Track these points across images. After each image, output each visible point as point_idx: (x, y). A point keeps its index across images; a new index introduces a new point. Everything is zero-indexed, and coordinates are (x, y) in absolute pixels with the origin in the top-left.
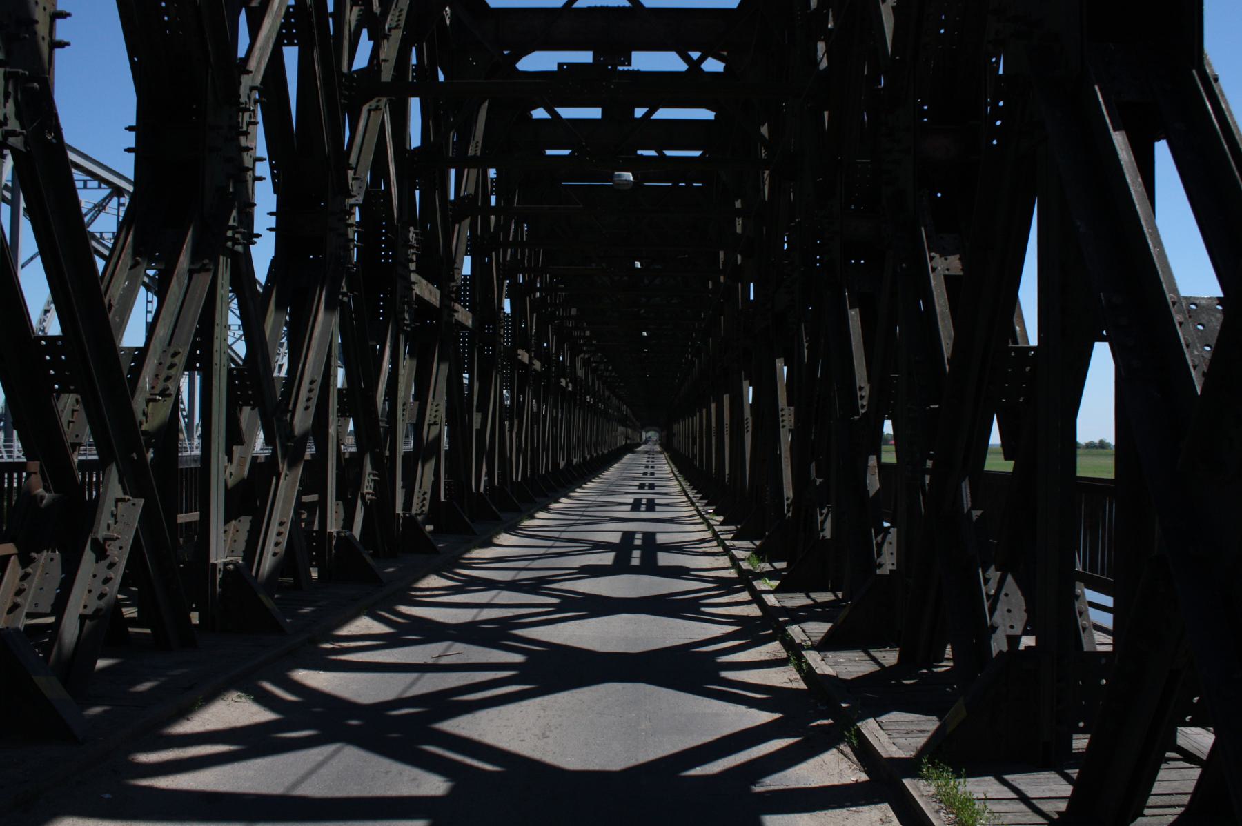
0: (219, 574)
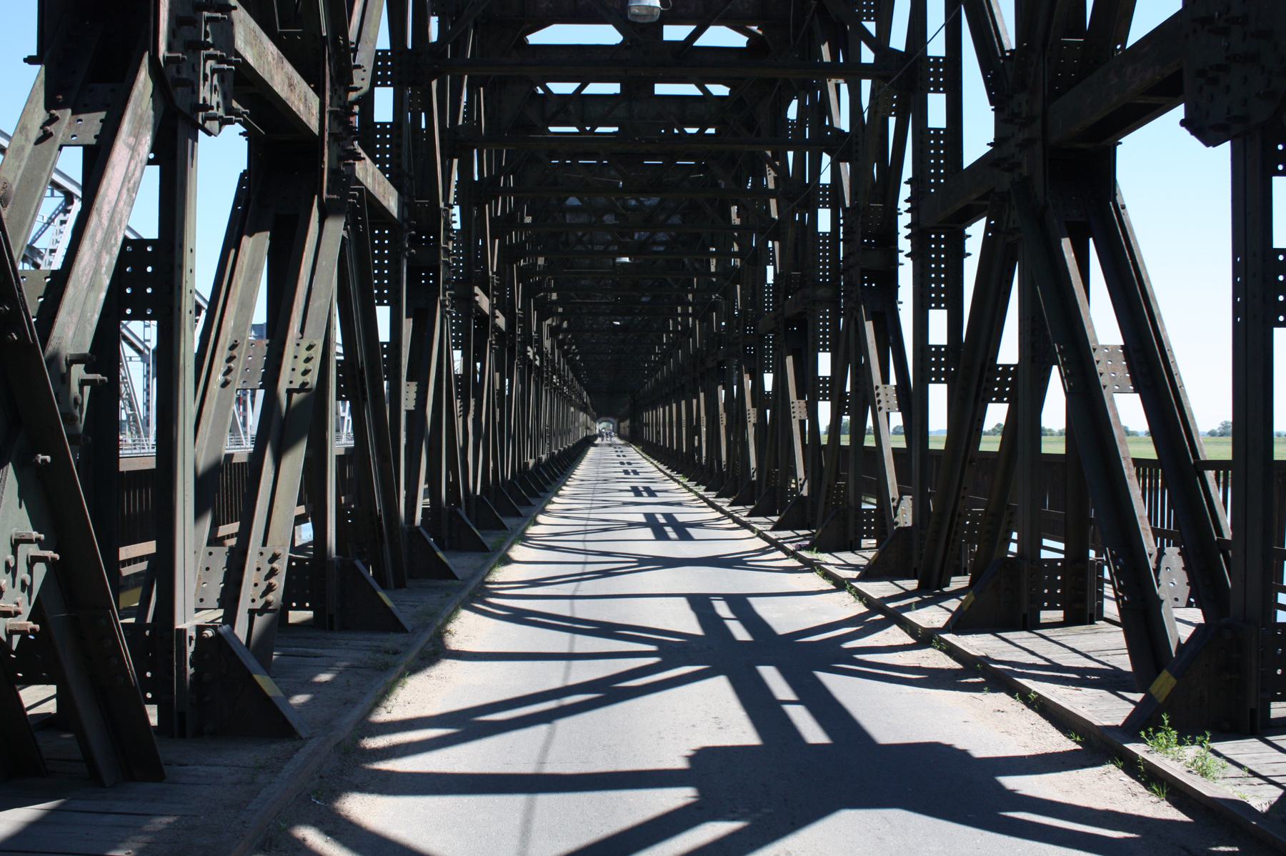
0: (190, 645)
